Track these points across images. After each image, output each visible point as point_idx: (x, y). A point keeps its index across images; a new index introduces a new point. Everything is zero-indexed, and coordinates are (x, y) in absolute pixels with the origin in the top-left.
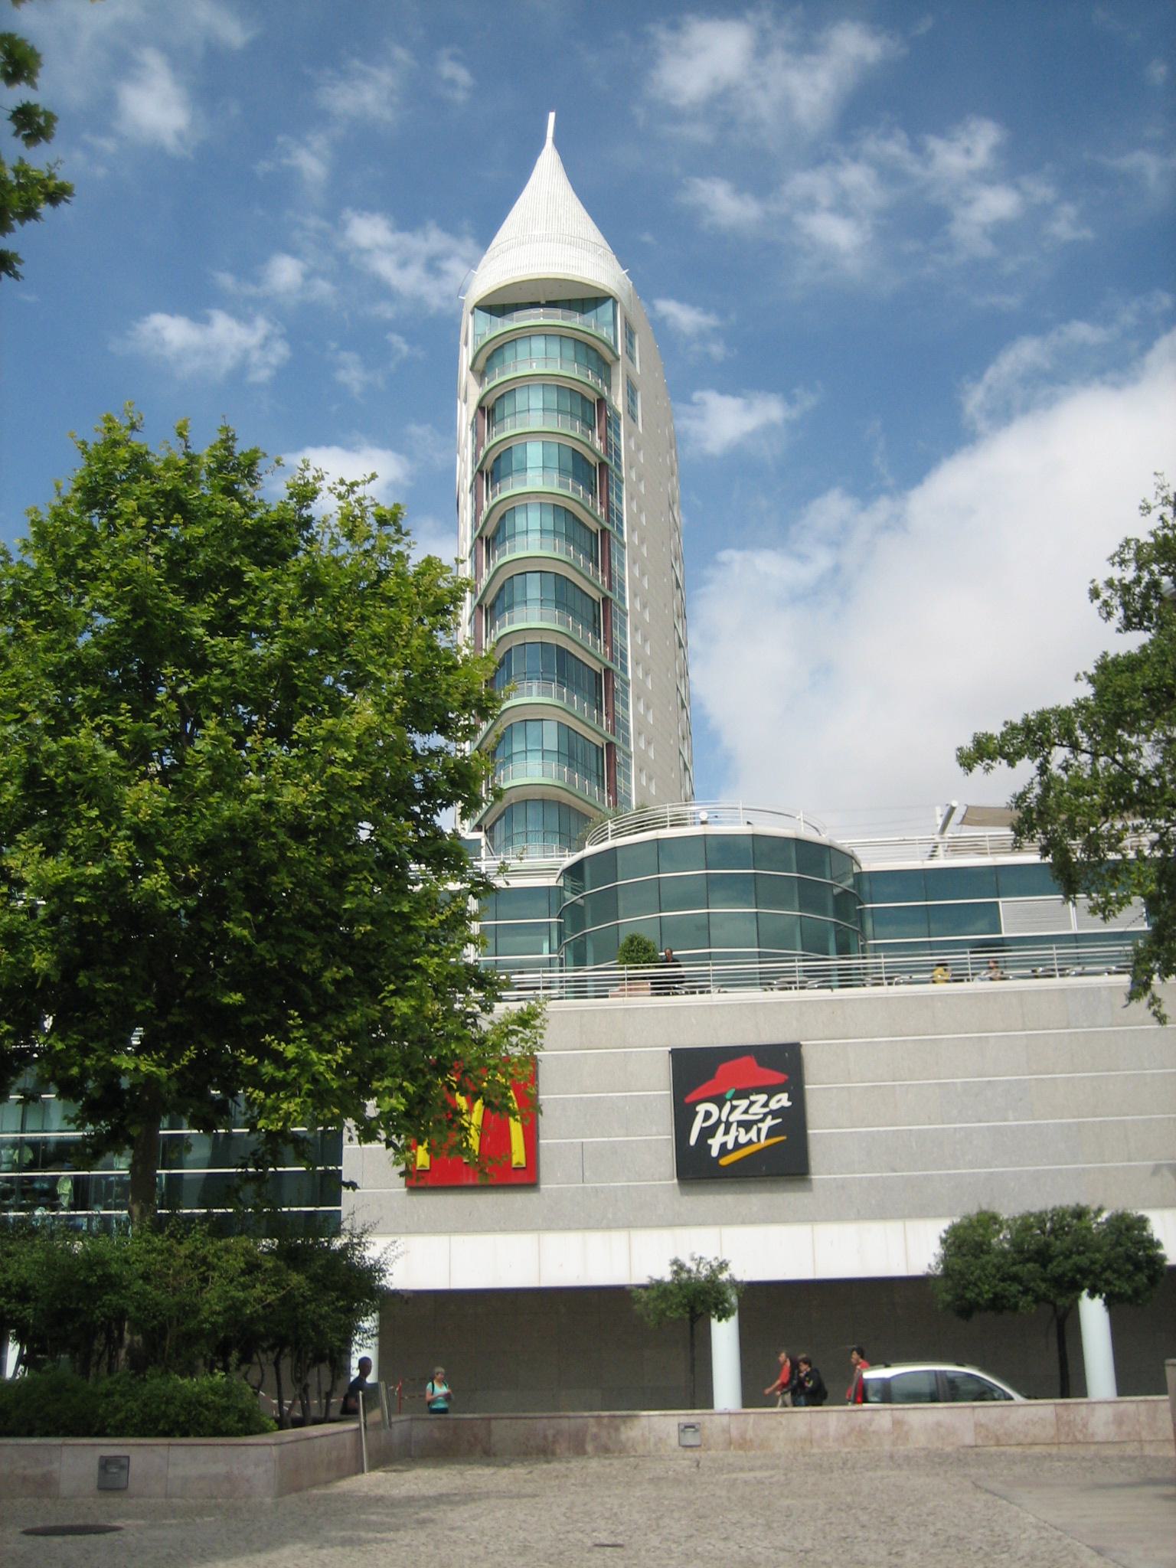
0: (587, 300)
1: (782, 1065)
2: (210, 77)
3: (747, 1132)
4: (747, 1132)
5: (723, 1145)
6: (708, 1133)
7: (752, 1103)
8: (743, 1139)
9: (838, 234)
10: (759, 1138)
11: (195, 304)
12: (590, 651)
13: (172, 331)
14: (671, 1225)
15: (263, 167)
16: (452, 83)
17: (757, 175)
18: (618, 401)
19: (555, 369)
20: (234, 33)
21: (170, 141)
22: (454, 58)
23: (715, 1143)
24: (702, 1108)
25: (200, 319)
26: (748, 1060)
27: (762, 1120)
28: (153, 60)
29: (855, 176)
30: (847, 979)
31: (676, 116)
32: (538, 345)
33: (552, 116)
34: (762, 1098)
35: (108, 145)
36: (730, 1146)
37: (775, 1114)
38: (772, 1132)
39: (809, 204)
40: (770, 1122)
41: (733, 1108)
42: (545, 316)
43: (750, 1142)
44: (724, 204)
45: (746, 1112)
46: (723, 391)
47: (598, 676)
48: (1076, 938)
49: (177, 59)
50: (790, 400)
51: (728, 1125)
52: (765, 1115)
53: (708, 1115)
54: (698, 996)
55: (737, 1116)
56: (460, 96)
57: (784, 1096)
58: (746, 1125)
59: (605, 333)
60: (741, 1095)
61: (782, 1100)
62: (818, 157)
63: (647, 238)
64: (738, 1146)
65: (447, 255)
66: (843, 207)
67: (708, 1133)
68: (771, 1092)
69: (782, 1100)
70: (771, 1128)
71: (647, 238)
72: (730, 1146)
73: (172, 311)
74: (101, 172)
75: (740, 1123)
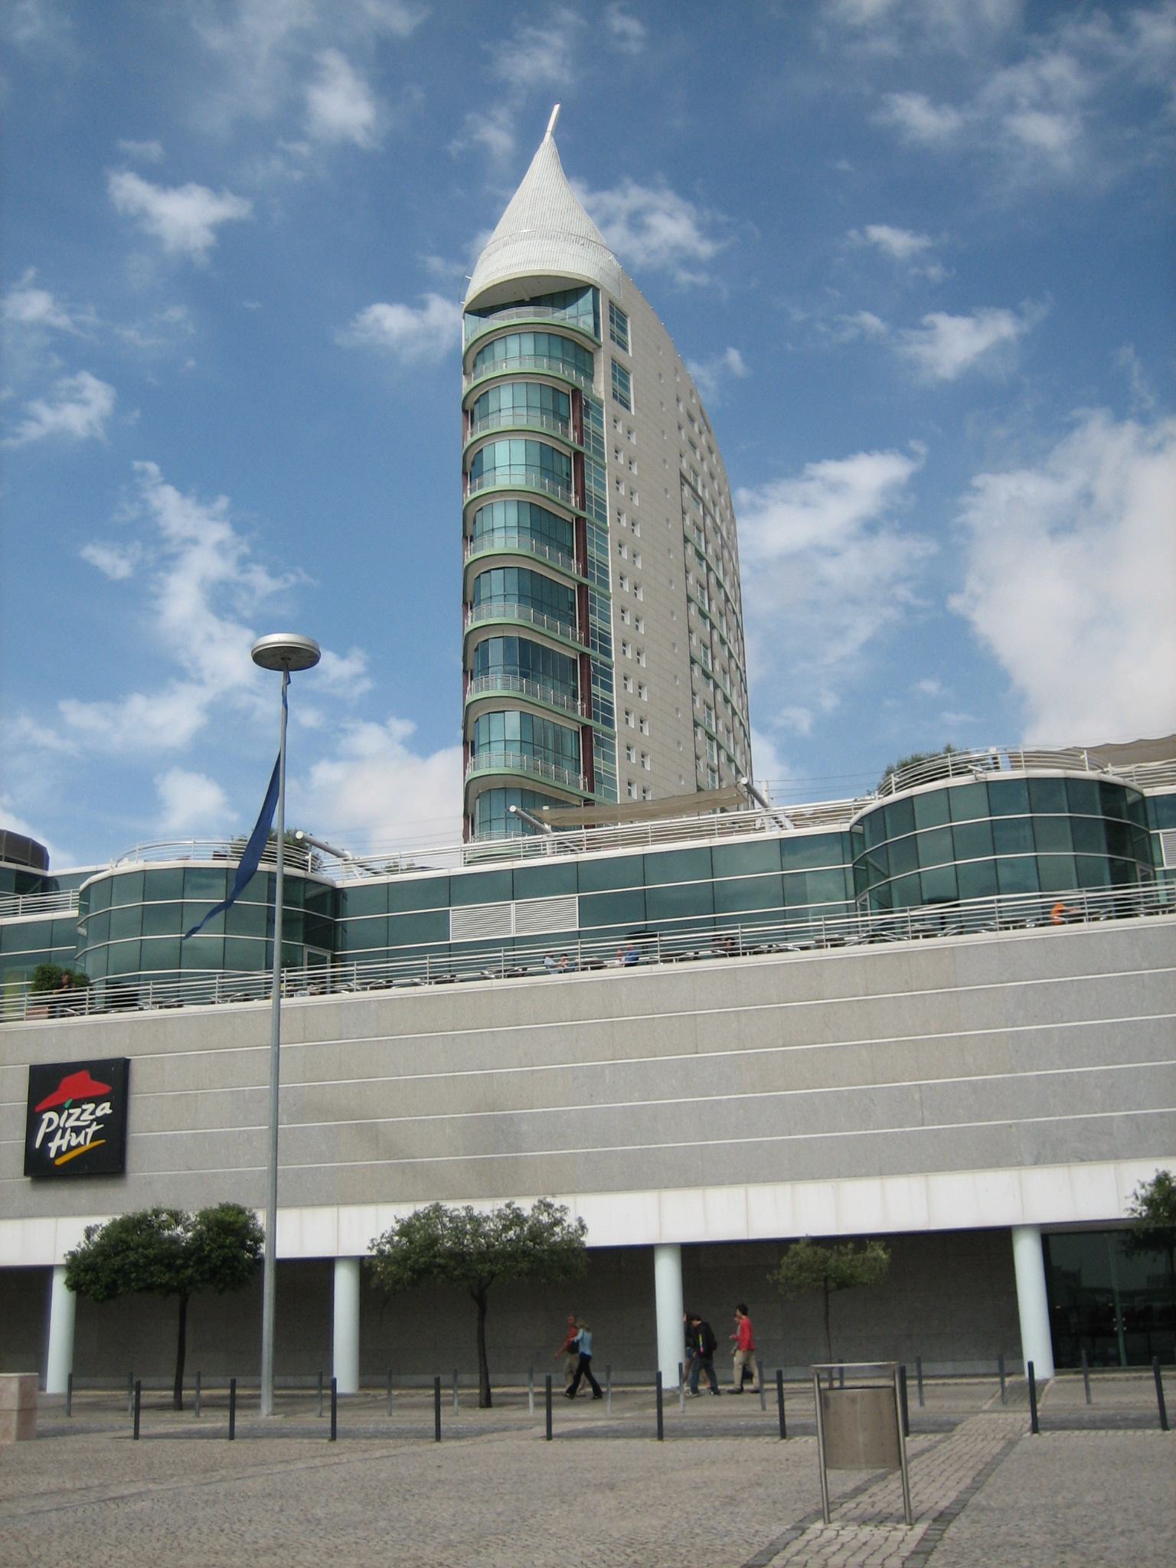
0: (563, 293)
1: (112, 1078)
2: (387, 67)
3: (77, 1136)
4: (77, 1136)
5: (59, 1148)
6: (49, 1137)
7: (83, 1111)
8: (73, 1143)
9: (1045, 131)
10: (84, 1142)
11: (409, 291)
12: (564, 641)
13: (391, 320)
14: (22, 1216)
15: (456, 146)
16: (623, 36)
17: (948, 83)
18: (601, 387)
19: (529, 367)
20: (402, 22)
21: (360, 138)
22: (624, 11)
23: (53, 1147)
24: (47, 1116)
25: (419, 306)
26: (85, 1074)
27: (88, 1126)
28: (333, 60)
29: (1058, 68)
30: (1125, 910)
31: (857, 35)
32: (513, 344)
33: (557, 107)
34: (91, 1107)
35: (303, 149)
36: (64, 1149)
37: (98, 1120)
38: (96, 1136)
39: (1011, 105)
40: (95, 1127)
41: (70, 1115)
42: (536, 315)
43: (79, 1145)
44: (920, 117)
45: (78, 1119)
46: (952, 313)
47: (575, 661)
48: (513, 941)
49: (354, 54)
50: (1019, 313)
51: (64, 1130)
52: (92, 1121)
53: (51, 1121)
54: (1011, 931)
55: (71, 1123)
56: (634, 48)
57: (108, 1105)
58: (77, 1130)
59: (586, 323)
60: (74, 1106)
61: (105, 1108)
62: (1013, 55)
63: (844, 165)
64: (70, 1148)
65: (651, 210)
66: (1045, 103)
67: (49, 1137)
68: (98, 1101)
69: (105, 1108)
70: (95, 1133)
71: (844, 165)
72: (64, 1149)
73: (391, 299)
74: (298, 175)
75: (73, 1128)
